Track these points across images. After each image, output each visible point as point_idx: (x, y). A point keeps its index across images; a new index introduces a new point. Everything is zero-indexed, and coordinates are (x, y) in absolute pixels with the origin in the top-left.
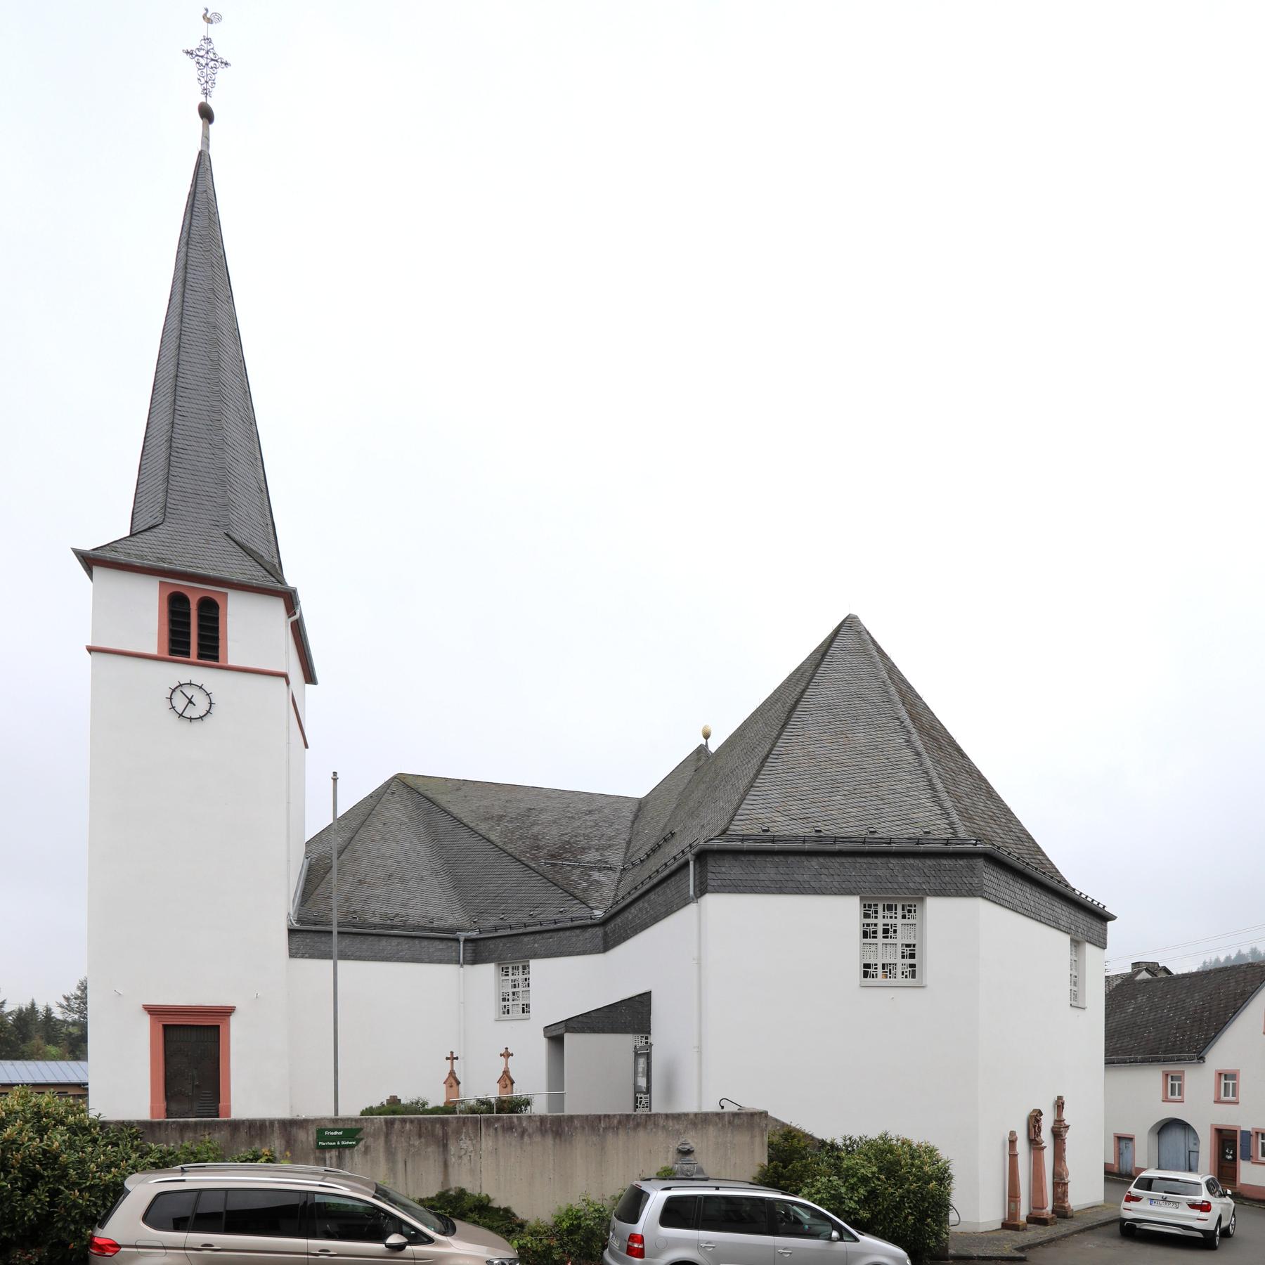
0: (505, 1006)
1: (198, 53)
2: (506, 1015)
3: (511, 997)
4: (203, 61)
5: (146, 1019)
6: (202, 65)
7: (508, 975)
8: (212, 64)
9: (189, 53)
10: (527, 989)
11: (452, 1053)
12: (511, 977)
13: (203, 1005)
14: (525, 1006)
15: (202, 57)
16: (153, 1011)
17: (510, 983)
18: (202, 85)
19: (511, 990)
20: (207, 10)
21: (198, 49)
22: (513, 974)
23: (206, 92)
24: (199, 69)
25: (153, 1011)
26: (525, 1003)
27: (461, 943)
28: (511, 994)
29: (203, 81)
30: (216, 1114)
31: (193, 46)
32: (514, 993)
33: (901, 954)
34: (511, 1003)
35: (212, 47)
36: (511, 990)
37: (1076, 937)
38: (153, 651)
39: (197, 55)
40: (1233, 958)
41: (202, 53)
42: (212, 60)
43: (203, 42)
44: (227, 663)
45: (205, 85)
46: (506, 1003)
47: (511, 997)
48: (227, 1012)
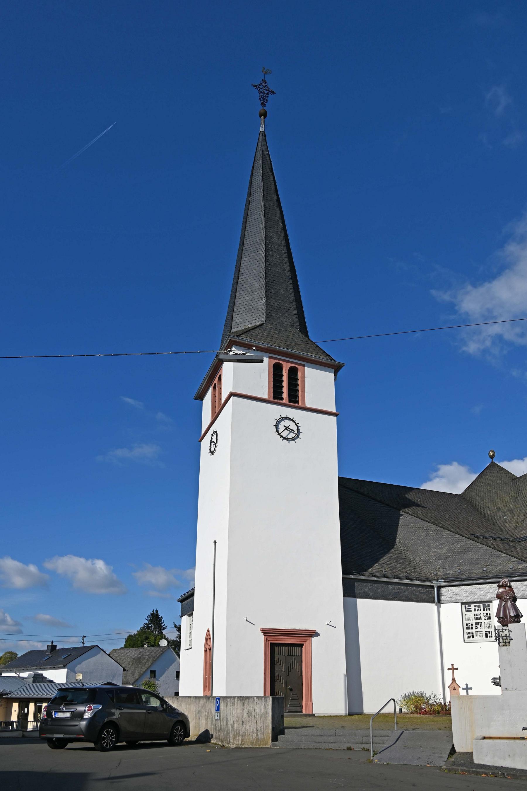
0: (469, 633)
1: (260, 87)
2: (471, 639)
3: (474, 626)
4: (261, 90)
5: (262, 637)
6: (261, 92)
7: (471, 611)
8: (266, 92)
9: (274, 93)
10: (489, 620)
11: (452, 665)
12: (473, 612)
13: (307, 629)
14: (488, 633)
15: (262, 88)
16: (266, 632)
17: (473, 617)
18: (261, 101)
19: (474, 622)
20: (264, 68)
21: (260, 85)
22: (475, 610)
23: (263, 104)
24: (260, 94)
25: (266, 632)
26: (488, 630)
27: (436, 588)
28: (474, 624)
29: (262, 99)
30: (299, 710)
31: (257, 83)
32: (476, 624)
33: (481, 610)
34: (474, 630)
35: (266, 84)
36: (474, 622)
37: (189, 614)
38: (266, 397)
39: (259, 88)
40: (18, 656)
41: (261, 87)
42: (266, 90)
43: (262, 82)
44: (305, 405)
45: (263, 101)
46: (470, 631)
47: (474, 626)
48: (314, 634)
